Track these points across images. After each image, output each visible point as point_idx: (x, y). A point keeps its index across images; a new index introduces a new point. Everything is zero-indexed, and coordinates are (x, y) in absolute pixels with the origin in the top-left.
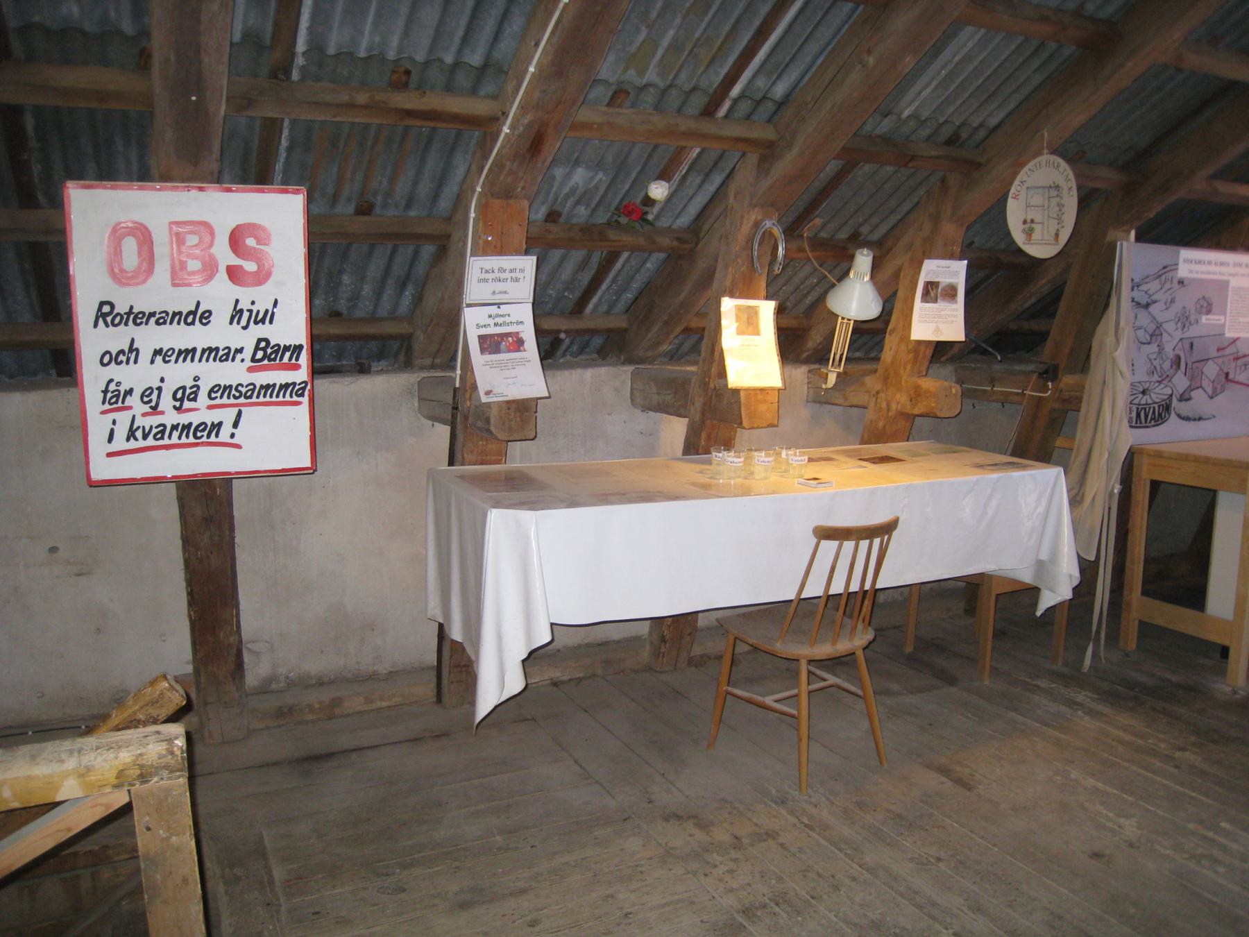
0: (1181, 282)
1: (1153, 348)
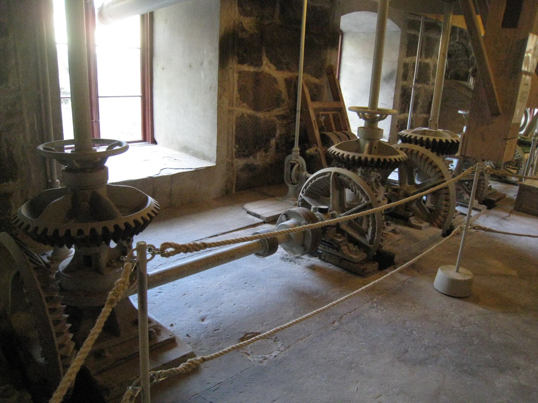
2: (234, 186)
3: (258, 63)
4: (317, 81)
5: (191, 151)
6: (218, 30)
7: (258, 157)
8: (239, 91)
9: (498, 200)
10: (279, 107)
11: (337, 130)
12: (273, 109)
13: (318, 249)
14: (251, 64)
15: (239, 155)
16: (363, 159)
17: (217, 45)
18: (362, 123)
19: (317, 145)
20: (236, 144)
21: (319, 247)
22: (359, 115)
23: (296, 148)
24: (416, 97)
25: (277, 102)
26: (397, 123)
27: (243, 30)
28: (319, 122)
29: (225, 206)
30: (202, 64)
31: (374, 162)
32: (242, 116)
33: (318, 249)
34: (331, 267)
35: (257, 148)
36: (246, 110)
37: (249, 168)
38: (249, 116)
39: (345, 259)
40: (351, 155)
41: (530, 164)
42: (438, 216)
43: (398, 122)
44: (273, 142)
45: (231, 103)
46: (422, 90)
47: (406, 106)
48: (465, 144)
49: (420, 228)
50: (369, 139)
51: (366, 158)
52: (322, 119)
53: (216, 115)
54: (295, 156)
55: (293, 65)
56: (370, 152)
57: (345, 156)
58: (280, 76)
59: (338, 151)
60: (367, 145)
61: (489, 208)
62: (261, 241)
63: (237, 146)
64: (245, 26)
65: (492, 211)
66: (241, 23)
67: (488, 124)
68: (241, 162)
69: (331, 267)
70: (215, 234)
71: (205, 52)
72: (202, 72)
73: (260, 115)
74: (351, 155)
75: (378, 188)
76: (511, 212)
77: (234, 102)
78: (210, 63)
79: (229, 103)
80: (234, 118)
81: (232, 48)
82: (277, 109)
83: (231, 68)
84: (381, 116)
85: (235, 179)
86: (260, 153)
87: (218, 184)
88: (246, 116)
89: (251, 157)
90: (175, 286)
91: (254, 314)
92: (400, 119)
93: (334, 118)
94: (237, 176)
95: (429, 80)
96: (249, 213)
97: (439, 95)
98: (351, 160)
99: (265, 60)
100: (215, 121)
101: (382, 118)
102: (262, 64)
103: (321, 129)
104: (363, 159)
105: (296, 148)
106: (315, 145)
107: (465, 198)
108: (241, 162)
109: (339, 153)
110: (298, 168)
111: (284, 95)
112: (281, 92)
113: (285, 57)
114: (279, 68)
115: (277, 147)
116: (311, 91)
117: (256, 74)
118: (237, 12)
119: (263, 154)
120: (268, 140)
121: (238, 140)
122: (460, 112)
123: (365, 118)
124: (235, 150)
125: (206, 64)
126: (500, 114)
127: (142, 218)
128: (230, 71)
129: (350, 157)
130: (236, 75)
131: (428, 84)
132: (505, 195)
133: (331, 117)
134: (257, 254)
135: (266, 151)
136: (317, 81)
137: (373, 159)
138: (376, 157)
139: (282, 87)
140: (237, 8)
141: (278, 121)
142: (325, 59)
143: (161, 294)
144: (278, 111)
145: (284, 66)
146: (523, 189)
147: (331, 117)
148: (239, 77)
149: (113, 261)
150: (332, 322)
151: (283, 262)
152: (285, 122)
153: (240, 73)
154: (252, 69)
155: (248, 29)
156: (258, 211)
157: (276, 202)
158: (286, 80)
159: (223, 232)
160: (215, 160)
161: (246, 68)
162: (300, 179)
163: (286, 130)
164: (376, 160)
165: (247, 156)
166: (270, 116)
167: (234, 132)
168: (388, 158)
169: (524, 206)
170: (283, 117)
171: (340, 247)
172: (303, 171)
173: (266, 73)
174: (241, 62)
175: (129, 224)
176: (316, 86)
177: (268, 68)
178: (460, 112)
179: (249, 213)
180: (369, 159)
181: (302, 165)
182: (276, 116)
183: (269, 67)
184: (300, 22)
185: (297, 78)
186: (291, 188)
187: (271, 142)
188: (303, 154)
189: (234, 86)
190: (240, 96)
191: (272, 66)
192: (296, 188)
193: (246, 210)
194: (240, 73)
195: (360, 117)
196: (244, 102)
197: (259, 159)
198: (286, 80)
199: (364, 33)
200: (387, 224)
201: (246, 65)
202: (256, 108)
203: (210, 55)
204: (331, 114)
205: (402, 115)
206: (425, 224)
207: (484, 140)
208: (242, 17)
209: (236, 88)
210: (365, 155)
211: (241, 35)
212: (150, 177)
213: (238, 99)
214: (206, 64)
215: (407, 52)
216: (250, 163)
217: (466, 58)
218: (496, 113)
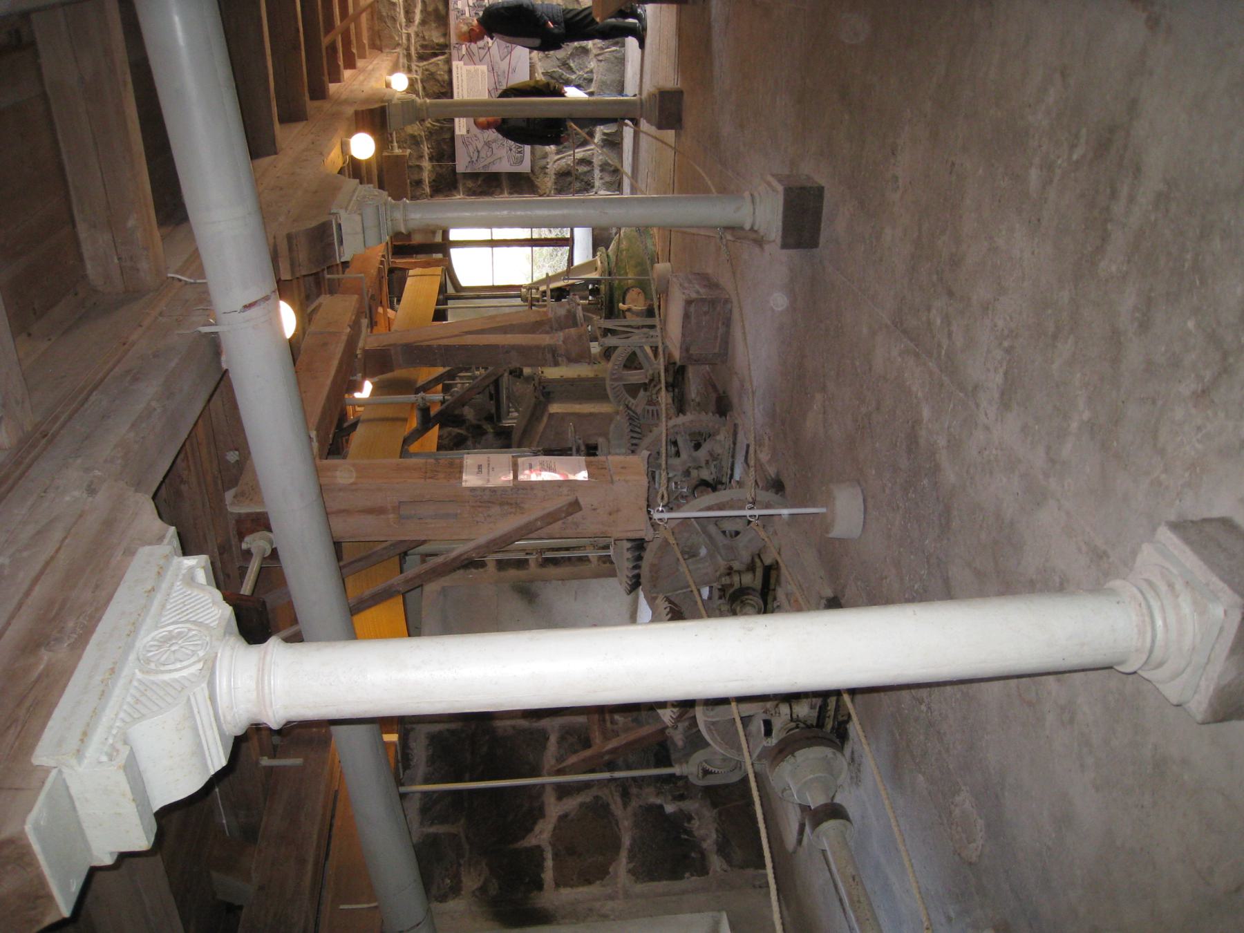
0: (468, 131)
1: (494, 145)
4: (553, 739)
8: (589, 882)
9: (714, 387)
10: (608, 804)
12: (613, 815)
14: (540, 866)
15: (703, 870)
25: (599, 810)
27: (483, 889)
32: (629, 871)
38: (631, 858)
54: (688, 769)
55: (535, 794)
58: (554, 808)
63: (687, 875)
64: (479, 884)
68: (716, 863)
70: (838, 904)
73: (626, 841)
82: (613, 807)
88: (631, 866)
96: (800, 841)
97: (473, 203)
99: (531, 841)
102: (538, 847)
108: (716, 863)
112: (582, 805)
113: (526, 809)
115: (681, 798)
136: (553, 739)
139: (571, 804)
144: (617, 808)
148: (566, 885)
153: (557, 885)
154: (549, 863)
155: (482, 879)
156: (795, 827)
158: (559, 798)
161: (548, 875)
169: (716, 351)
170: (625, 795)
174: (539, 886)
176: (562, 739)
177: (542, 835)
179: (800, 841)
183: (541, 832)
190: (598, 879)
191: (537, 828)
194: (557, 885)
196: (608, 873)
201: (543, 876)
211: (493, 890)
212: (249, 453)
216: (715, 848)
218: (575, 506)
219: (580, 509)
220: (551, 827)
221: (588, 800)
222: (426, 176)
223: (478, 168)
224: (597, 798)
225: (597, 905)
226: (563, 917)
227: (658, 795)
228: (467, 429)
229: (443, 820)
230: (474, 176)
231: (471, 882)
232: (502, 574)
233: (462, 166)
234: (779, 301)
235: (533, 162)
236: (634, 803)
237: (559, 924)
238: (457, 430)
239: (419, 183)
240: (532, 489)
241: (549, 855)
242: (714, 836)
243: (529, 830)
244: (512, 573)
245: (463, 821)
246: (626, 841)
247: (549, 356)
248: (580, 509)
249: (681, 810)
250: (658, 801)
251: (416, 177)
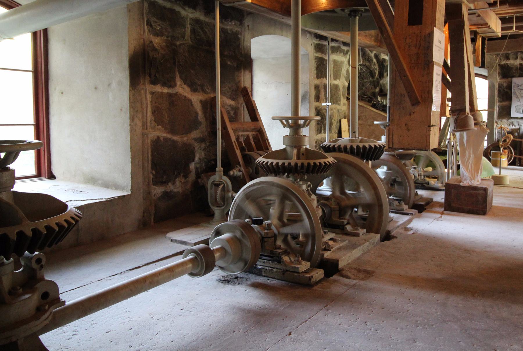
2: (153, 217)
3: (170, 83)
5: (100, 182)
6: (127, 48)
7: (178, 183)
8: (153, 112)
11: (258, 150)
13: (257, 265)
14: (164, 85)
15: (158, 181)
16: (293, 164)
17: (126, 63)
18: (287, 131)
19: (240, 166)
20: (152, 169)
21: (258, 263)
22: (283, 124)
23: (219, 168)
24: (331, 118)
25: (194, 124)
26: (315, 144)
27: (154, 49)
28: (239, 143)
29: (144, 238)
30: (109, 85)
31: (304, 166)
33: (257, 265)
34: (273, 282)
35: (176, 173)
36: (161, 133)
37: (167, 195)
38: (166, 139)
39: (287, 271)
40: (280, 162)
41: (450, 167)
42: (373, 221)
43: (316, 142)
44: (192, 166)
45: (144, 125)
46: (334, 110)
47: (321, 127)
48: (391, 137)
49: (357, 235)
50: (295, 147)
51: (296, 164)
52: (242, 140)
53: (129, 139)
56: (298, 158)
57: (274, 164)
59: (266, 160)
60: (295, 151)
61: (420, 212)
62: (196, 258)
63: (154, 172)
65: (424, 214)
66: (151, 42)
67: (410, 114)
68: (158, 191)
69: (273, 282)
71: (113, 72)
72: (110, 94)
73: (176, 138)
74: (280, 162)
75: (310, 197)
76: (442, 213)
77: (149, 124)
78: (120, 83)
79: (143, 126)
80: (149, 141)
81: (143, 67)
83: (143, 89)
84: (305, 123)
85: (153, 209)
86: (179, 179)
87: (135, 213)
88: (161, 139)
89: (170, 184)
90: (94, 325)
91: (197, 339)
92: (317, 139)
93: (254, 138)
94: (156, 206)
95: (340, 101)
98: (280, 167)
99: (179, 82)
100: (129, 145)
101: (304, 126)
102: (176, 85)
103: (242, 150)
104: (293, 164)
105: (219, 168)
106: (238, 166)
107: (395, 205)
108: (158, 191)
109: (268, 162)
110: (223, 189)
111: (201, 116)
114: (194, 90)
116: (228, 113)
117: (170, 95)
118: (146, 31)
119: (183, 180)
120: (187, 166)
121: (155, 165)
122: (375, 123)
123: (290, 126)
124: (152, 176)
125: (114, 85)
126: (419, 102)
127: (57, 224)
128: (143, 92)
129: (280, 164)
130: (149, 96)
131: (339, 104)
132: (432, 199)
133: (251, 138)
134: (192, 274)
135: (186, 177)
137: (302, 164)
138: (306, 162)
139: (198, 107)
140: (146, 27)
141: (196, 144)
142: (240, 81)
143: (76, 336)
144: (195, 134)
145: (199, 88)
146: (449, 189)
147: (251, 138)
148: (152, 98)
149: (18, 288)
150: (288, 333)
151: (221, 284)
152: (203, 145)
153: (153, 93)
154: (166, 90)
157: (202, 228)
159: (146, 262)
160: (130, 188)
161: (158, 89)
162: (226, 201)
163: (205, 154)
164: (306, 164)
165: (165, 182)
166: (187, 140)
167: (150, 156)
168: (317, 161)
170: (201, 140)
171: (280, 258)
172: (228, 191)
173: (181, 95)
174: (154, 82)
175: (39, 231)
177: (181, 89)
178: (375, 123)
180: (299, 165)
181: (227, 184)
182: (194, 139)
183: (183, 88)
184: (213, 44)
185: (214, 99)
186: (217, 212)
187: (190, 167)
188: (226, 173)
189: (147, 107)
190: (155, 119)
191: (185, 87)
192: (223, 210)
193: (169, 238)
194: (153, 93)
195: (285, 126)
197: (177, 187)
198: (201, 102)
199: (273, 58)
200: (325, 233)
202: (173, 131)
203: (120, 75)
204: (250, 134)
205: (319, 135)
206: (362, 232)
207: (408, 130)
208: (151, 36)
209: (149, 110)
210: (294, 160)
213: (153, 122)
214: (114, 85)
215: (317, 74)
216: (168, 190)
217: (371, 79)
218: (415, 102)
219: (413, 105)
220: (186, 95)
221: (199, 118)
222: (511, 62)
223: (514, 89)
224: (200, 123)
225: (140, 116)
226: (134, 95)
227: (200, 159)
228: (377, 78)
229: (193, 31)
230: (510, 86)
231: (157, 41)
232: (313, 88)
233: (516, 81)
234: (272, 211)
235: (516, 118)
236: (196, 145)
237: (130, 91)
238: (377, 73)
239: (507, 58)
240: (428, 74)
241: (170, 91)
242: (175, 190)
243: (185, 81)
244: (313, 93)
245: (190, 42)
246: (176, 138)
247: (458, 107)
248: (413, 105)
249: (191, 172)
250: (196, 159)
251: (511, 56)
